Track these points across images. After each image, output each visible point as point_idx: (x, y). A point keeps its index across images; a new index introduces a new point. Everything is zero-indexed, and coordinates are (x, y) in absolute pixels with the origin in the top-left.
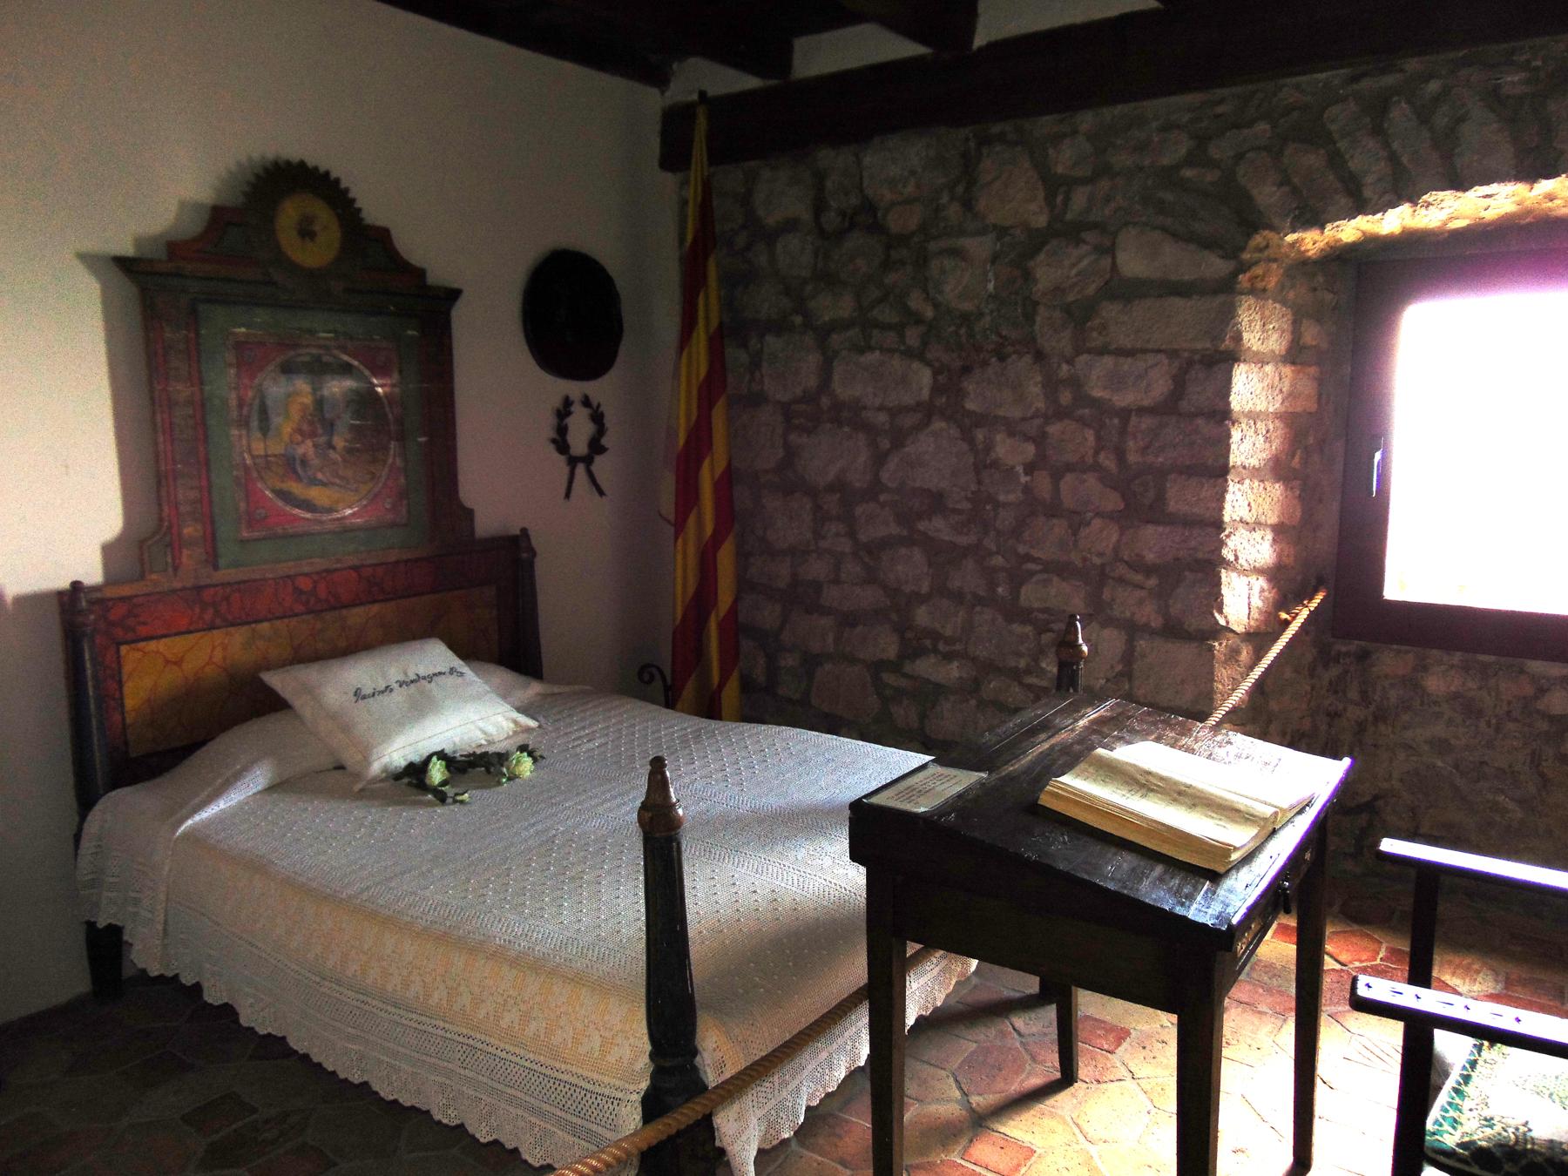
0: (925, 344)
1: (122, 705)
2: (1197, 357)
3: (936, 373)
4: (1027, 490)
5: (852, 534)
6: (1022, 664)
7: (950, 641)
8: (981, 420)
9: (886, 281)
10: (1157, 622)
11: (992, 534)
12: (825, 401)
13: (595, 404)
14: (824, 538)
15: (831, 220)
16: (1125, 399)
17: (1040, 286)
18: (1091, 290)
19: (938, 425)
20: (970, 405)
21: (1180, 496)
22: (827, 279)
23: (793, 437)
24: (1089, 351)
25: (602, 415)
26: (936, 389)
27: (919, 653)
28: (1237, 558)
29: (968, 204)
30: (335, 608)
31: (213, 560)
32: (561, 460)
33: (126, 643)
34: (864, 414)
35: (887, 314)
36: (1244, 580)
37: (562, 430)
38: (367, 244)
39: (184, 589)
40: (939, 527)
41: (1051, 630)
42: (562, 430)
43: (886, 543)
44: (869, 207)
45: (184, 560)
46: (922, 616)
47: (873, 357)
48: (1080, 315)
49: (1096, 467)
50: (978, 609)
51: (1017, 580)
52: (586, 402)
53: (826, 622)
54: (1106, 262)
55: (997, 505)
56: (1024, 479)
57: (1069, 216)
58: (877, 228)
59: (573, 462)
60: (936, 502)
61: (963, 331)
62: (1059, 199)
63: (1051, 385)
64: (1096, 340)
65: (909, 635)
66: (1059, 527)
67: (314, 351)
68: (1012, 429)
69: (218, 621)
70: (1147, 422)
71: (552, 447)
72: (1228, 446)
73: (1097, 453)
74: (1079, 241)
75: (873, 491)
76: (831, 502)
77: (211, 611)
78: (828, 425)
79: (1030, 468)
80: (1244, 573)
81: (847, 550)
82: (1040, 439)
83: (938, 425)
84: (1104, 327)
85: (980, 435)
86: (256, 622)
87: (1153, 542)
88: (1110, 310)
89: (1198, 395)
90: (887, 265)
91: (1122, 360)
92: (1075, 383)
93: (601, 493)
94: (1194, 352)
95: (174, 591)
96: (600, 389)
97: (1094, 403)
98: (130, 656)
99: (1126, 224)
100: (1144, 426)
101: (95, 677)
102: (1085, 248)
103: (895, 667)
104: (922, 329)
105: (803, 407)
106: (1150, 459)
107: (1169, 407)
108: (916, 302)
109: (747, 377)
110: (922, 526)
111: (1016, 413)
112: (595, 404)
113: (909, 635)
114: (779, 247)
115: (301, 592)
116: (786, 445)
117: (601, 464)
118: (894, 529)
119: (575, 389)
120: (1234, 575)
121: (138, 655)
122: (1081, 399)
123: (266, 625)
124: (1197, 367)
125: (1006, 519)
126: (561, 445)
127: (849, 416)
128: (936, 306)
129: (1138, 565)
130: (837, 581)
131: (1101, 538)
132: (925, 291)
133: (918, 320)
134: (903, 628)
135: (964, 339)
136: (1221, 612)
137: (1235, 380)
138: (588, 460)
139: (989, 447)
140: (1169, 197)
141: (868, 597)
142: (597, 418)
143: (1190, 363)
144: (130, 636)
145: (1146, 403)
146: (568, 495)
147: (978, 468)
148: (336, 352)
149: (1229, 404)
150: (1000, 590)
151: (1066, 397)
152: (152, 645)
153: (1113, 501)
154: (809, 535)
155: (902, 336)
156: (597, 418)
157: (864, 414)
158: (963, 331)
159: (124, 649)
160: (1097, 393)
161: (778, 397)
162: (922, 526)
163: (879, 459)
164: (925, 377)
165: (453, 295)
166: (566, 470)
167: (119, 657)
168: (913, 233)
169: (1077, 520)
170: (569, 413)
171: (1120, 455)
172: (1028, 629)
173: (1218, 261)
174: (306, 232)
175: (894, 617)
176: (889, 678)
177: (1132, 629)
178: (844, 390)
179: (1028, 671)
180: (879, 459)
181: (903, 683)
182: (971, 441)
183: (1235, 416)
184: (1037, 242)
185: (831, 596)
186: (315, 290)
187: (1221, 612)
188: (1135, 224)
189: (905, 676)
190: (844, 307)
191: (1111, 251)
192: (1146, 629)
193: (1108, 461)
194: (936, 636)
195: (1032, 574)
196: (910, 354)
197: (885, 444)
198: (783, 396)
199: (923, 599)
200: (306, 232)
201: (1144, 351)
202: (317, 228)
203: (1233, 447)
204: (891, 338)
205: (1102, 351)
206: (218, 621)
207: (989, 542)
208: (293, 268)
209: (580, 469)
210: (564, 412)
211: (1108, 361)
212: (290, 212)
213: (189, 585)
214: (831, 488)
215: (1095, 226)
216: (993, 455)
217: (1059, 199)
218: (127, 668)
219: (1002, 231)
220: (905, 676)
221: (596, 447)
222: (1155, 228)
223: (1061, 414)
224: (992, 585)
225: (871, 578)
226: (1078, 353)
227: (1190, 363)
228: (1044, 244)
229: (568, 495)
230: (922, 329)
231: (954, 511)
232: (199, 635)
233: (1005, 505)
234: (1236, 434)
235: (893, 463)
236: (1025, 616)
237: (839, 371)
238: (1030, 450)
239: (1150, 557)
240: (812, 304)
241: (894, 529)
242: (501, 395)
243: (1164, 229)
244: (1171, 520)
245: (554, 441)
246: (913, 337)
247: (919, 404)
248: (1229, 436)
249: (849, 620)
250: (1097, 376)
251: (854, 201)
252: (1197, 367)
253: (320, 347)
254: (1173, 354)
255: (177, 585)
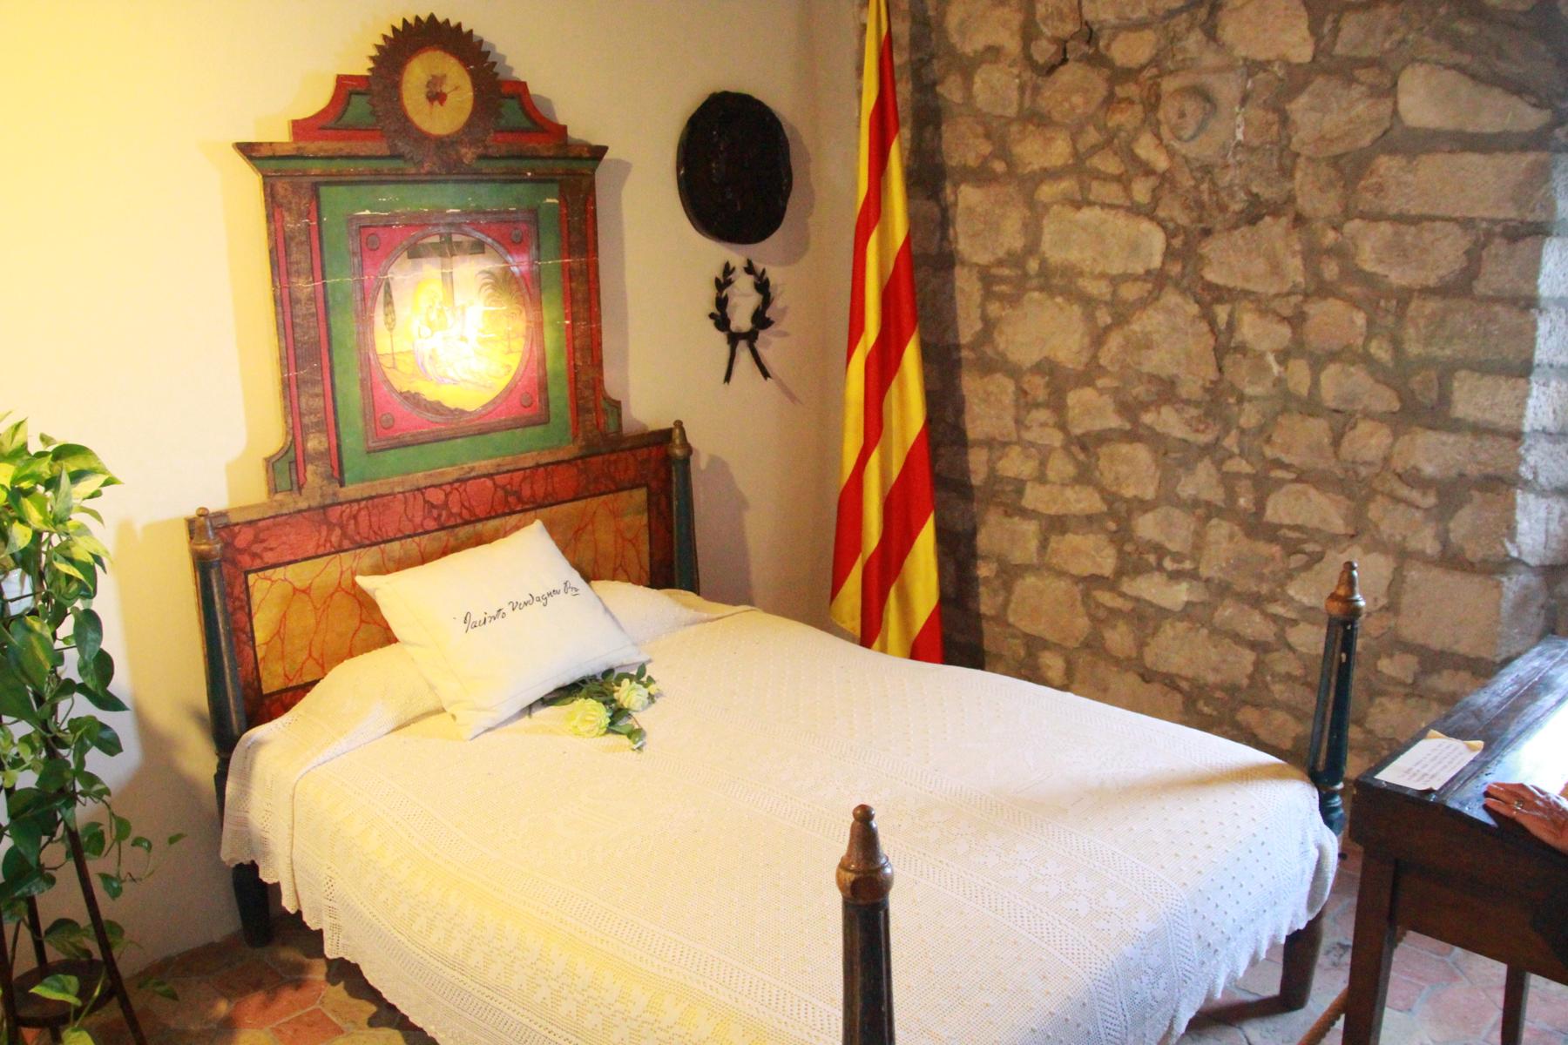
0: (1156, 200)
1: (253, 638)
2: (1498, 229)
3: (1170, 235)
4: (1279, 381)
5: (1063, 426)
6: (1265, 589)
7: (1178, 557)
8: (1220, 294)
9: (1110, 124)
10: (1431, 547)
11: (1234, 432)
12: (1033, 265)
13: (760, 271)
14: (1028, 428)
15: (1043, 51)
16: (1398, 276)
17: (1301, 134)
18: (1366, 141)
19: (1171, 298)
20: (1211, 276)
21: (1473, 398)
22: (1037, 119)
23: (994, 309)
24: (1363, 216)
25: (767, 282)
26: (1169, 253)
27: (1139, 570)
28: (1535, 474)
29: (1211, 34)
30: (467, 523)
31: (338, 474)
32: (720, 338)
33: (256, 571)
34: (1081, 282)
35: (1110, 164)
36: (1543, 503)
37: (722, 303)
38: (498, 93)
39: (309, 509)
40: (1169, 421)
41: (1303, 552)
42: (722, 303)
43: (1103, 437)
44: (1090, 35)
45: (309, 476)
46: (1147, 527)
47: (1088, 215)
48: (1350, 169)
49: (1367, 359)
50: (1214, 521)
51: (1263, 486)
52: (750, 269)
53: (1030, 528)
54: (1385, 107)
55: (1241, 399)
56: (1276, 369)
57: (1339, 50)
58: (1098, 60)
59: (734, 339)
60: (1167, 391)
61: (1204, 187)
62: (1326, 29)
63: (1312, 255)
64: (1367, 200)
65: (1129, 548)
66: (1318, 429)
67: (442, 230)
68: (1263, 307)
69: (346, 544)
70: (1433, 305)
71: (711, 322)
72: (1533, 340)
73: (1368, 338)
74: (1351, 81)
75: (1087, 376)
76: (1038, 387)
77: (338, 531)
78: (1036, 295)
79: (1284, 356)
80: (1542, 493)
81: (1057, 444)
82: (1297, 320)
83: (1171, 298)
84: (1380, 189)
85: (1222, 313)
86: (385, 542)
87: (1432, 453)
88: (1387, 165)
89: (1496, 276)
90: (1110, 101)
91: (1403, 228)
92: (1340, 252)
93: (766, 375)
94: (1493, 221)
95: (300, 511)
96: (765, 253)
97: (1369, 279)
98: (259, 585)
99: (1413, 60)
100: (1427, 311)
101: (225, 610)
102: (1357, 91)
103: (1111, 584)
104: (1152, 182)
105: (1006, 272)
106: (1435, 351)
107: (1459, 287)
108: (1146, 148)
109: (938, 235)
110: (1148, 418)
111: (1269, 288)
112: (760, 271)
113: (1129, 548)
114: (978, 80)
115: (433, 506)
116: (985, 318)
117: (771, 346)
118: (1114, 422)
119: (735, 255)
120: (1531, 497)
121: (267, 584)
122: (1352, 273)
123: (396, 545)
124: (1497, 240)
125: (1249, 417)
126: (721, 320)
127: (1059, 282)
128: (1171, 153)
129: (1413, 478)
130: (1041, 479)
131: (1369, 442)
132: (1158, 136)
133: (1148, 171)
134: (1122, 536)
135: (1205, 197)
136: (1512, 541)
137: (1545, 258)
138: (751, 337)
139: (1231, 326)
140: (1467, 29)
141: (1084, 501)
142: (762, 286)
143: (1489, 235)
144: (258, 563)
145: (1432, 282)
146: (728, 378)
147: (1220, 352)
148: (467, 229)
149: (1536, 287)
150: (1242, 501)
151: (1331, 270)
152: (279, 573)
153: (1386, 400)
154: (1011, 424)
155: (1127, 189)
156: (762, 286)
157: (1081, 282)
158: (1204, 187)
159: (252, 577)
160: (1369, 267)
161: (975, 259)
162: (1148, 418)
163: (1098, 339)
164: (1157, 240)
165: (599, 153)
166: (725, 349)
167: (247, 588)
168: (1142, 68)
169: (1342, 421)
170: (729, 283)
171: (1396, 344)
172: (1276, 549)
173: (1530, 110)
174: (436, 97)
175: (1112, 526)
176: (1105, 598)
177: (1404, 556)
178: (1054, 251)
179: (1273, 599)
180: (1098, 339)
181: (1118, 603)
182: (1208, 317)
183: (1542, 304)
184: (1296, 80)
185: (1033, 497)
186: (443, 160)
187: (1512, 541)
188: (1423, 61)
189: (1123, 595)
190: (1059, 151)
191: (1391, 91)
192: (1420, 556)
193: (1380, 351)
194: (1160, 551)
195: (1280, 483)
196: (1135, 210)
197: (1104, 318)
198: (983, 258)
199: (1145, 506)
200: (436, 97)
201: (1433, 219)
202: (446, 89)
203: (1540, 341)
204: (1112, 192)
205: (1374, 217)
206: (346, 544)
207: (1230, 442)
208: (422, 137)
209: (743, 354)
210: (724, 282)
211: (1385, 228)
212: (417, 74)
213: (314, 504)
214: (1037, 369)
215: (1370, 63)
216: (1238, 337)
217: (1326, 29)
218: (257, 597)
219: (1254, 67)
220: (1123, 595)
221: (761, 320)
222: (1448, 67)
223: (1323, 290)
224: (1231, 495)
225: (1084, 477)
226: (1348, 214)
227: (1489, 235)
228: (1307, 83)
229: (728, 378)
230: (1152, 182)
231: (1187, 402)
232: (326, 558)
233: (1251, 399)
234: (1543, 326)
235: (1115, 341)
236: (1271, 533)
237: (1049, 229)
238: (1285, 331)
239: (1429, 470)
240: (1018, 150)
241: (1114, 422)
242: (656, 250)
243: (1462, 69)
244: (1456, 426)
245: (712, 316)
246: (1141, 191)
247: (1148, 272)
248: (1535, 327)
249: (1057, 524)
250: (1369, 246)
251: (1070, 28)
252: (1497, 240)
253: (450, 225)
254: (1466, 223)
255: (303, 505)
